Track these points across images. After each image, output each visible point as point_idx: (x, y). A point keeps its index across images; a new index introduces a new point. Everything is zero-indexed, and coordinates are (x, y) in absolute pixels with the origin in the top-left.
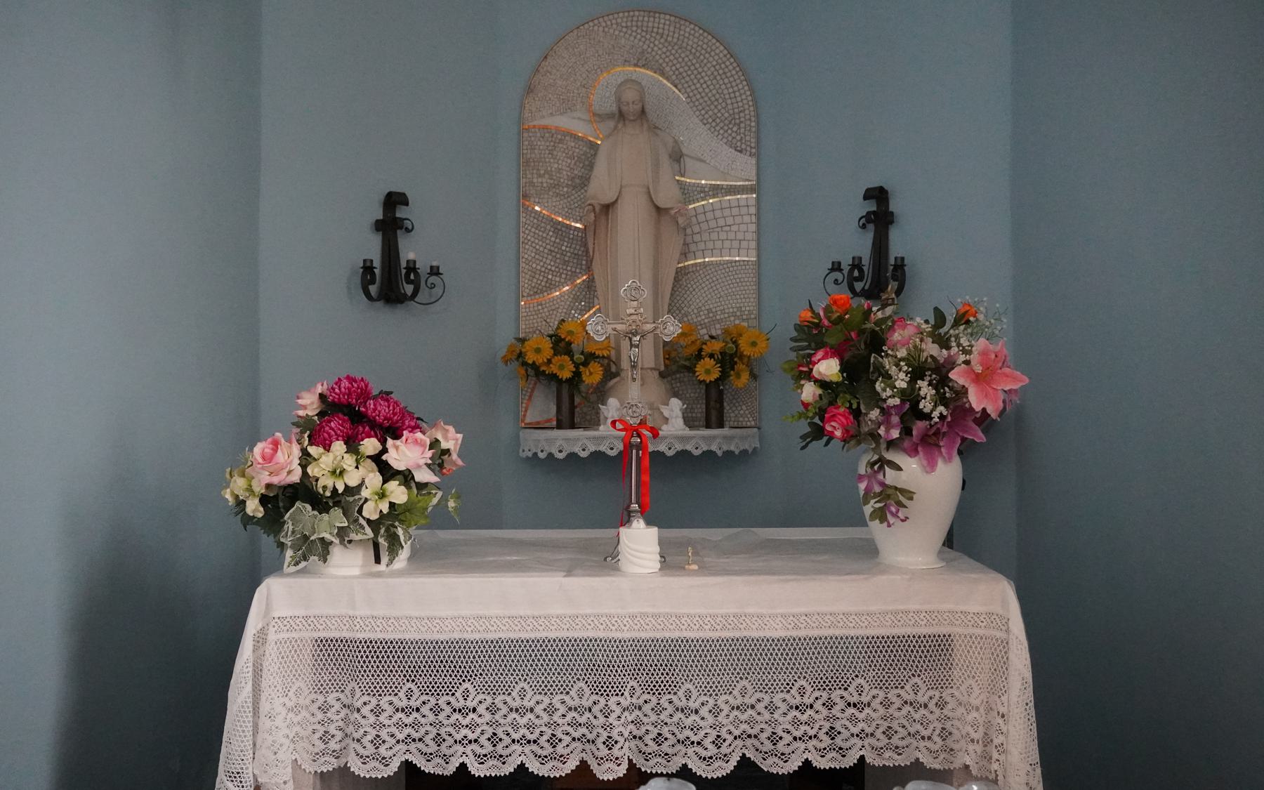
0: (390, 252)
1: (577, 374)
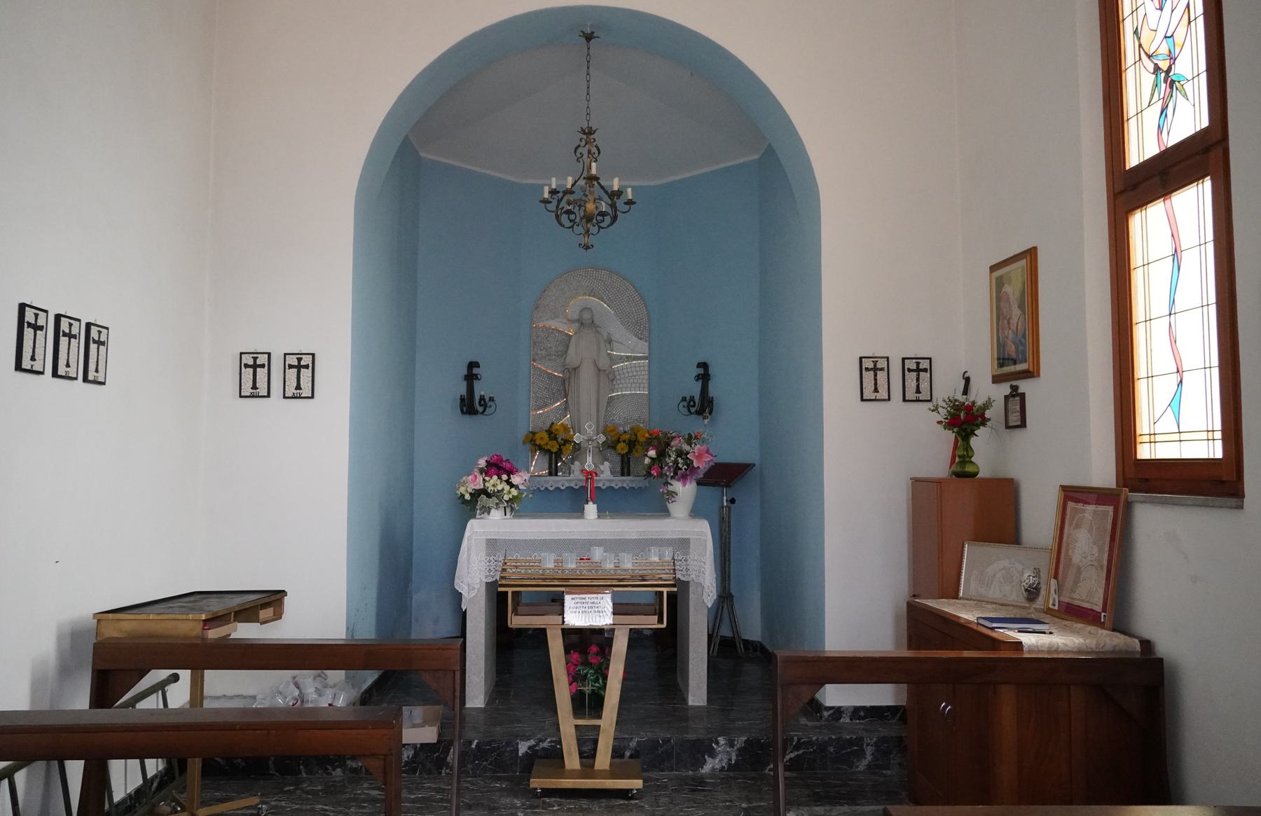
0: (470, 390)
1: (560, 450)
